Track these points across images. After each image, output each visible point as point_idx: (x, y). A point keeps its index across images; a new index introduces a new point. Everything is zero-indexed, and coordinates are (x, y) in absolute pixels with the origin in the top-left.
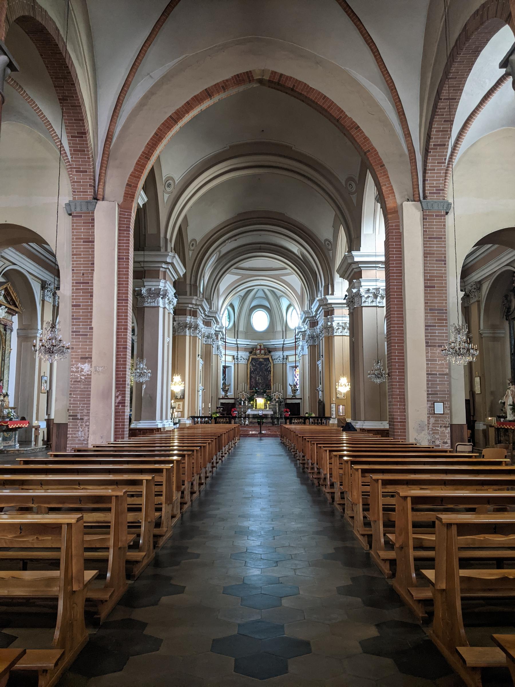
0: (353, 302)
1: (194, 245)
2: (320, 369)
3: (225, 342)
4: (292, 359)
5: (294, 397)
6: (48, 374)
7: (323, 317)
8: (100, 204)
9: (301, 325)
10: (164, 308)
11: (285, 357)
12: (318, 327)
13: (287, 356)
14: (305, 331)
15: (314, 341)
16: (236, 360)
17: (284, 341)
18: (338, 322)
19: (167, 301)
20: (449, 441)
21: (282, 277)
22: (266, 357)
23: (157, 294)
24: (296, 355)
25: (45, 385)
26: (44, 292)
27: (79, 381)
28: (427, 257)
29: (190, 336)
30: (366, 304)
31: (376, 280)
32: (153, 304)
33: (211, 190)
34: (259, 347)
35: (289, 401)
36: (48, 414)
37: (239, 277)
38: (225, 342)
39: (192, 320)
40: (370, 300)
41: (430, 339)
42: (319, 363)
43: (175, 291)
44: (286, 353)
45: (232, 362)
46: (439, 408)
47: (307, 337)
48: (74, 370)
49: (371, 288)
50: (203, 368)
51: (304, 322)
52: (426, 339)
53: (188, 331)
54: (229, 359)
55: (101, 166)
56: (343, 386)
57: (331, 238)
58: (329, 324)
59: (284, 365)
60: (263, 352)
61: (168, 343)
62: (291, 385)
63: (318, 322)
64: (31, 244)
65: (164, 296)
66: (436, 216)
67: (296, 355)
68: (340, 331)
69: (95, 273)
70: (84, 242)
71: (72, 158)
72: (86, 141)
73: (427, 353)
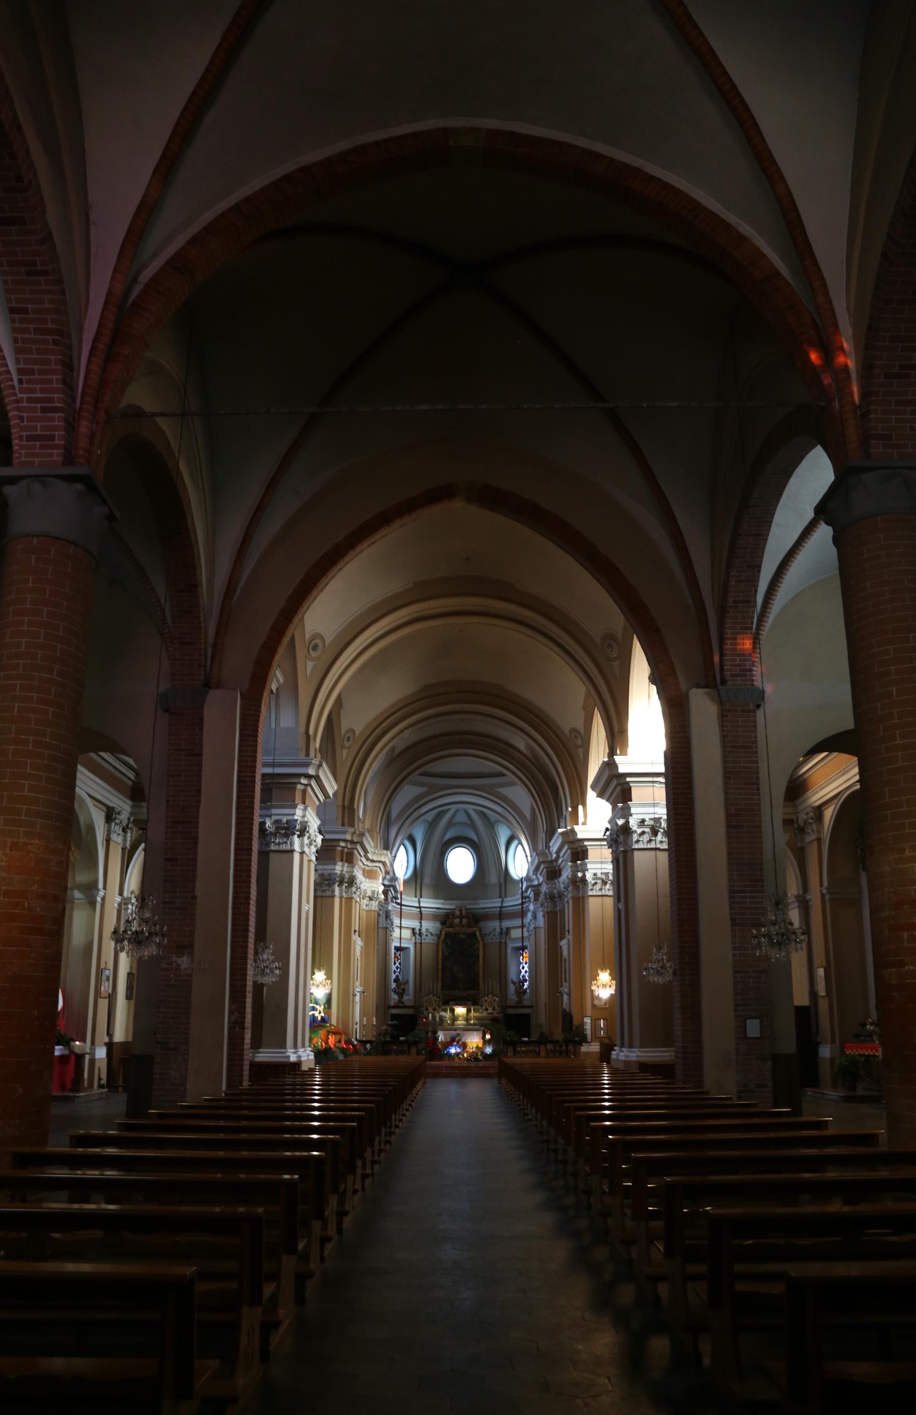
1: (351, 739)
2: (565, 953)
4: (516, 933)
10: (302, 853)
11: (504, 930)
14: (539, 885)
16: (418, 937)
17: (502, 902)
18: (595, 871)
19: (306, 841)
22: (470, 930)
23: (288, 829)
25: (107, 984)
26: (110, 827)
29: (341, 897)
30: (641, 846)
31: (654, 805)
34: (457, 913)
35: (511, 1011)
36: (110, 1033)
37: (425, 789)
38: (401, 905)
39: (345, 869)
40: (646, 838)
42: (563, 943)
44: (507, 924)
45: (410, 940)
46: (753, 1028)
49: (647, 817)
50: (361, 952)
52: (731, 914)
53: (337, 889)
54: (407, 934)
56: (604, 987)
58: (580, 874)
59: (503, 946)
60: (465, 921)
62: (514, 983)
64: (103, 754)
65: (303, 832)
68: (598, 886)
71: (20, 382)
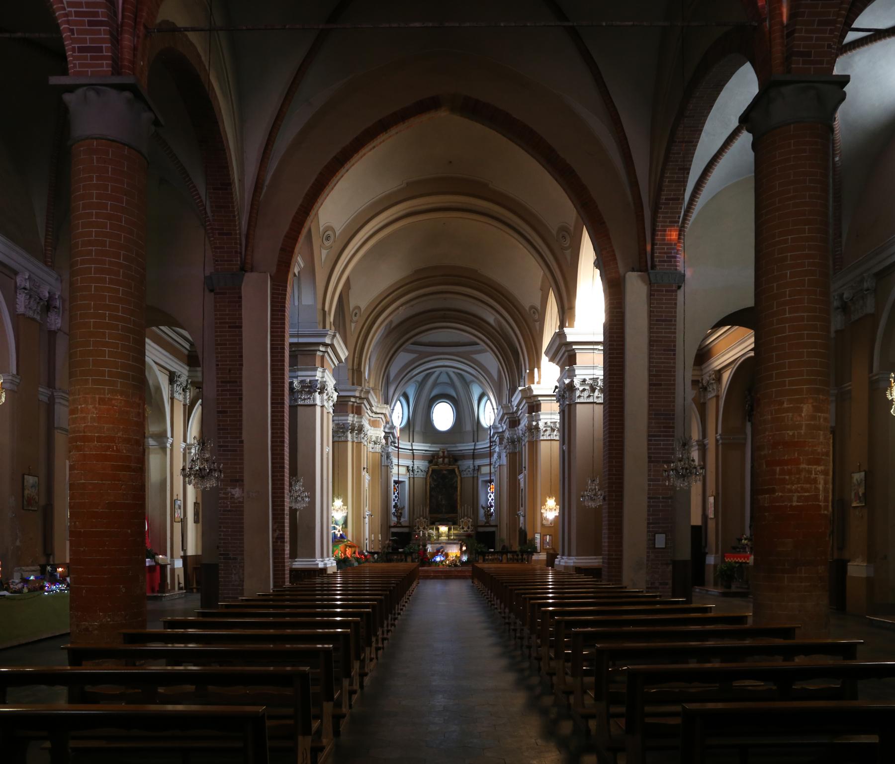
2: (522, 485)
3: (398, 448)
4: (485, 470)
5: (487, 524)
8: (248, 275)
9: (497, 423)
10: (322, 407)
12: (520, 427)
14: (503, 432)
15: (515, 447)
17: (475, 445)
19: (325, 397)
20: (670, 582)
22: (451, 467)
23: (311, 388)
24: (490, 464)
26: (173, 387)
27: (229, 511)
29: (353, 442)
31: (594, 367)
32: (308, 402)
34: (441, 454)
35: (481, 530)
36: (184, 548)
38: (398, 448)
40: (586, 394)
43: (334, 382)
44: (478, 462)
46: (660, 541)
47: (505, 441)
48: (222, 495)
49: (587, 378)
51: (501, 419)
53: (349, 435)
54: (403, 470)
56: (550, 510)
57: (538, 305)
60: (446, 460)
62: (483, 508)
63: (519, 420)
64: (161, 327)
65: (322, 390)
66: (667, 291)
67: (490, 464)
68: (548, 433)
69: (244, 368)
70: (229, 327)
72: (232, 194)
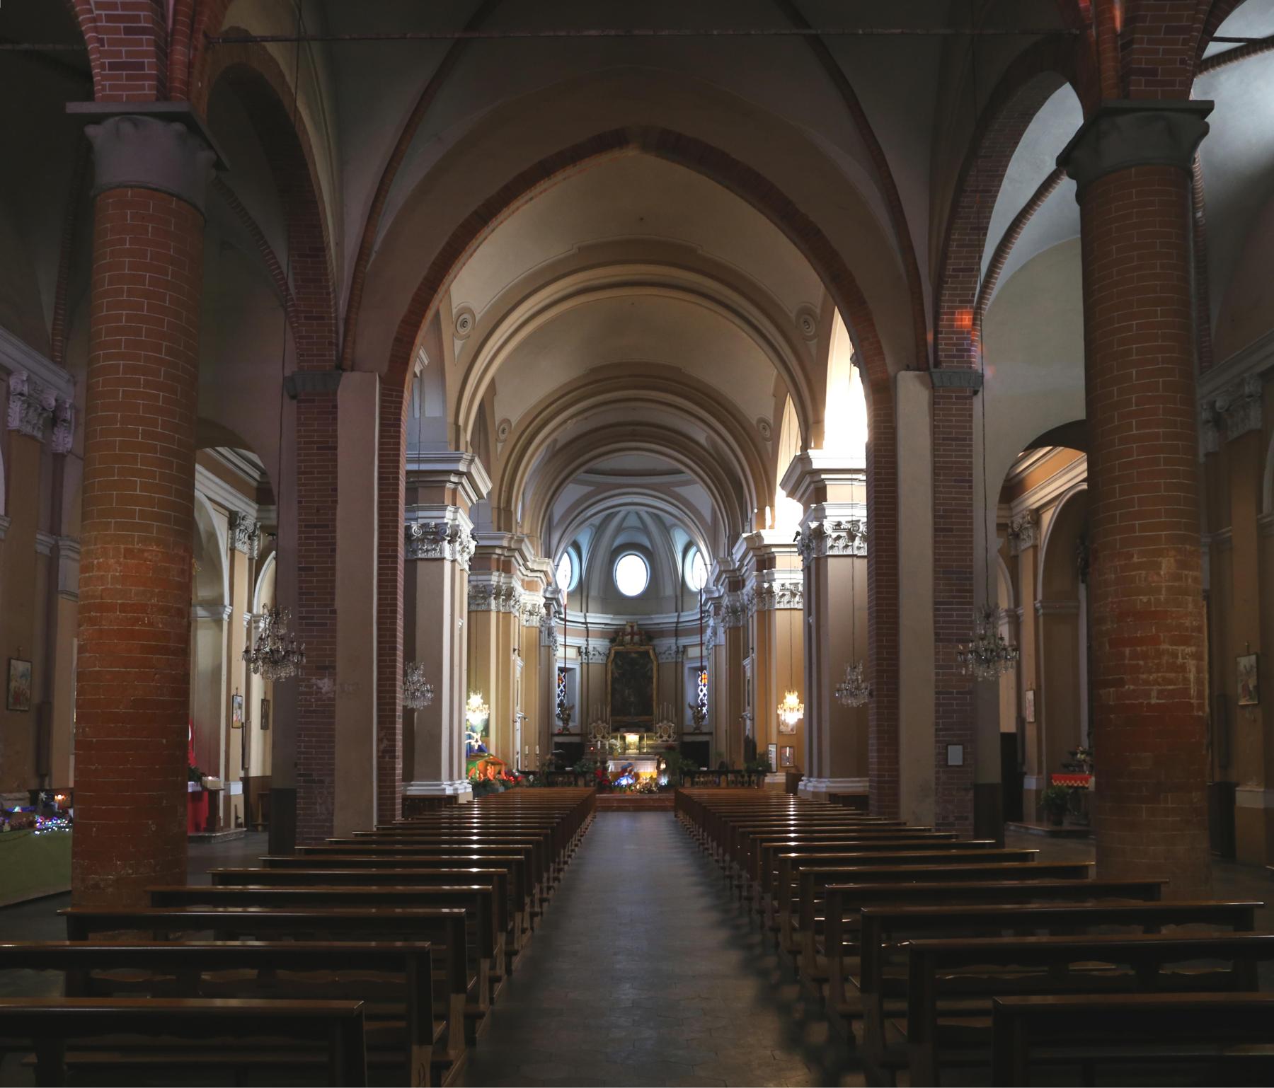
0: (812, 544)
2: (749, 674)
4: (694, 652)
6: (243, 692)
7: (755, 573)
9: (711, 585)
10: (454, 561)
12: (744, 591)
13: (684, 647)
14: (720, 597)
15: (738, 619)
19: (458, 548)
20: (971, 816)
21: (677, 489)
22: (643, 648)
23: (437, 534)
24: (701, 644)
26: (234, 534)
28: (939, 475)
29: (498, 612)
30: (835, 552)
31: (852, 505)
32: (432, 555)
33: (541, 329)
34: (628, 629)
35: (688, 739)
36: (245, 767)
38: (565, 620)
39: (502, 580)
40: (841, 543)
41: (942, 628)
42: (747, 662)
44: (683, 641)
46: (955, 755)
49: (843, 520)
53: (493, 602)
54: (572, 653)
55: (350, 306)
56: (791, 710)
57: (770, 417)
60: (636, 638)
61: (461, 629)
62: (691, 707)
63: (744, 581)
64: (219, 449)
65: (454, 537)
66: (957, 398)
67: (701, 644)
68: (786, 599)
69: (339, 507)
70: (318, 448)
73: (937, 653)
